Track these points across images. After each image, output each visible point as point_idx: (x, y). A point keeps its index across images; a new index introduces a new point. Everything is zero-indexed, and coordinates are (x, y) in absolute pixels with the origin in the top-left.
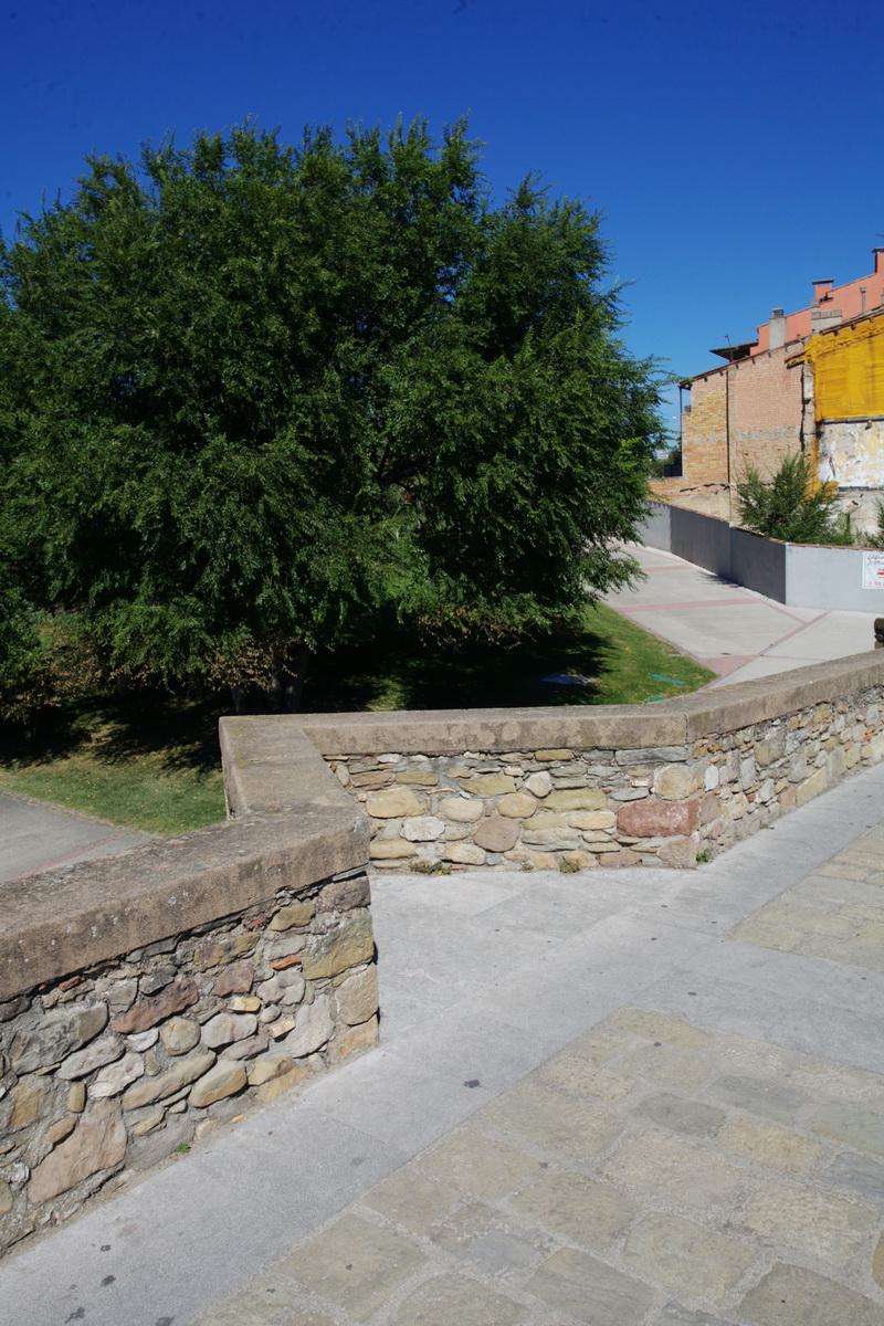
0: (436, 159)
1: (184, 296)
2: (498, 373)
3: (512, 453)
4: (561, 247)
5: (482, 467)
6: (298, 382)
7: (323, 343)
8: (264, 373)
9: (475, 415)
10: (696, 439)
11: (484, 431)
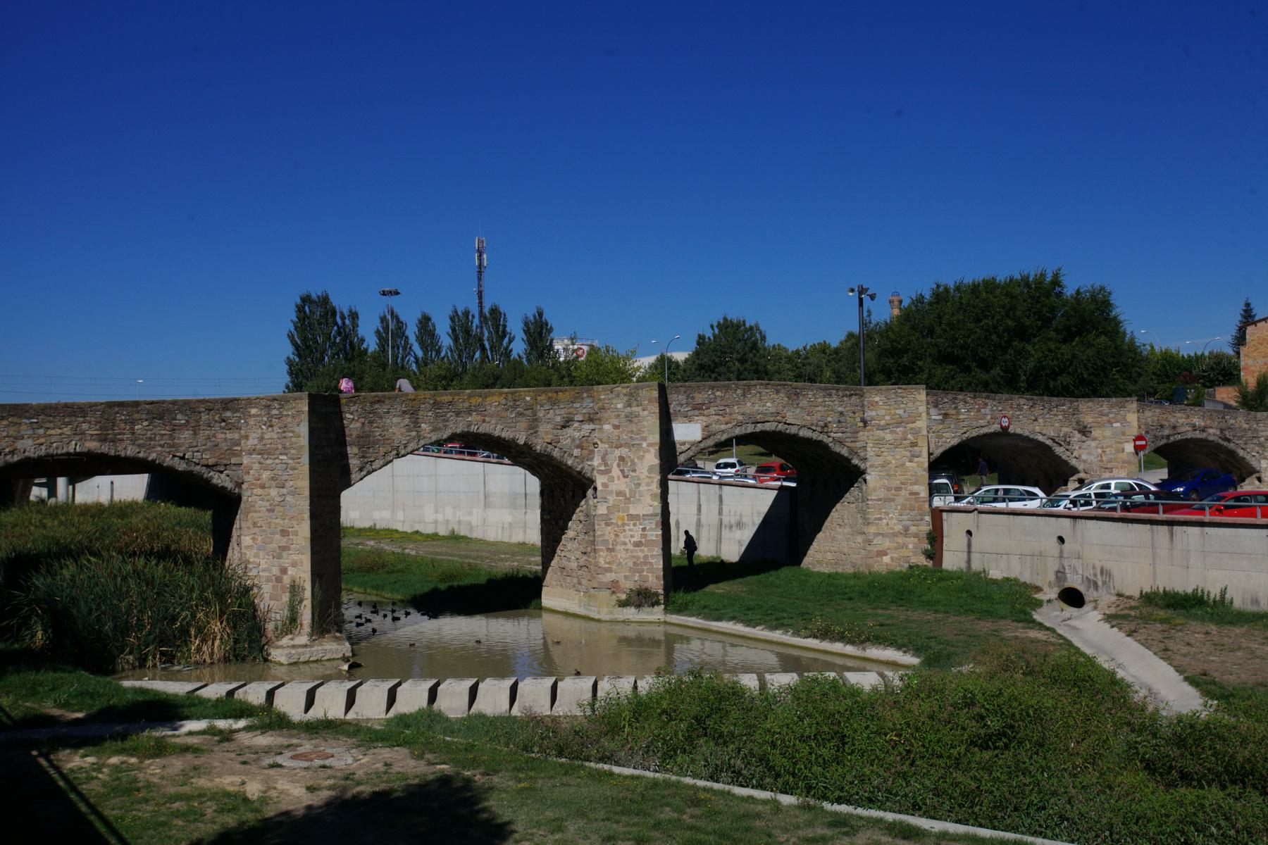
0: (1049, 278)
1: (969, 330)
2: (1065, 349)
3: (1069, 373)
4: (639, 683)
5: (1059, 378)
6: (1000, 353)
7: (1009, 342)
8: (991, 351)
9: (1055, 362)
10: (1250, 362)
11: (1058, 366)
